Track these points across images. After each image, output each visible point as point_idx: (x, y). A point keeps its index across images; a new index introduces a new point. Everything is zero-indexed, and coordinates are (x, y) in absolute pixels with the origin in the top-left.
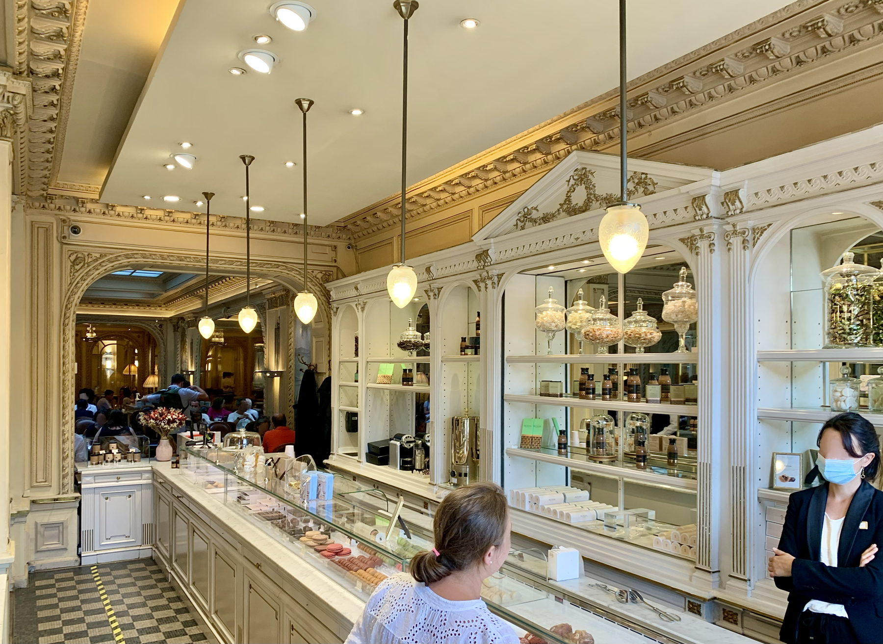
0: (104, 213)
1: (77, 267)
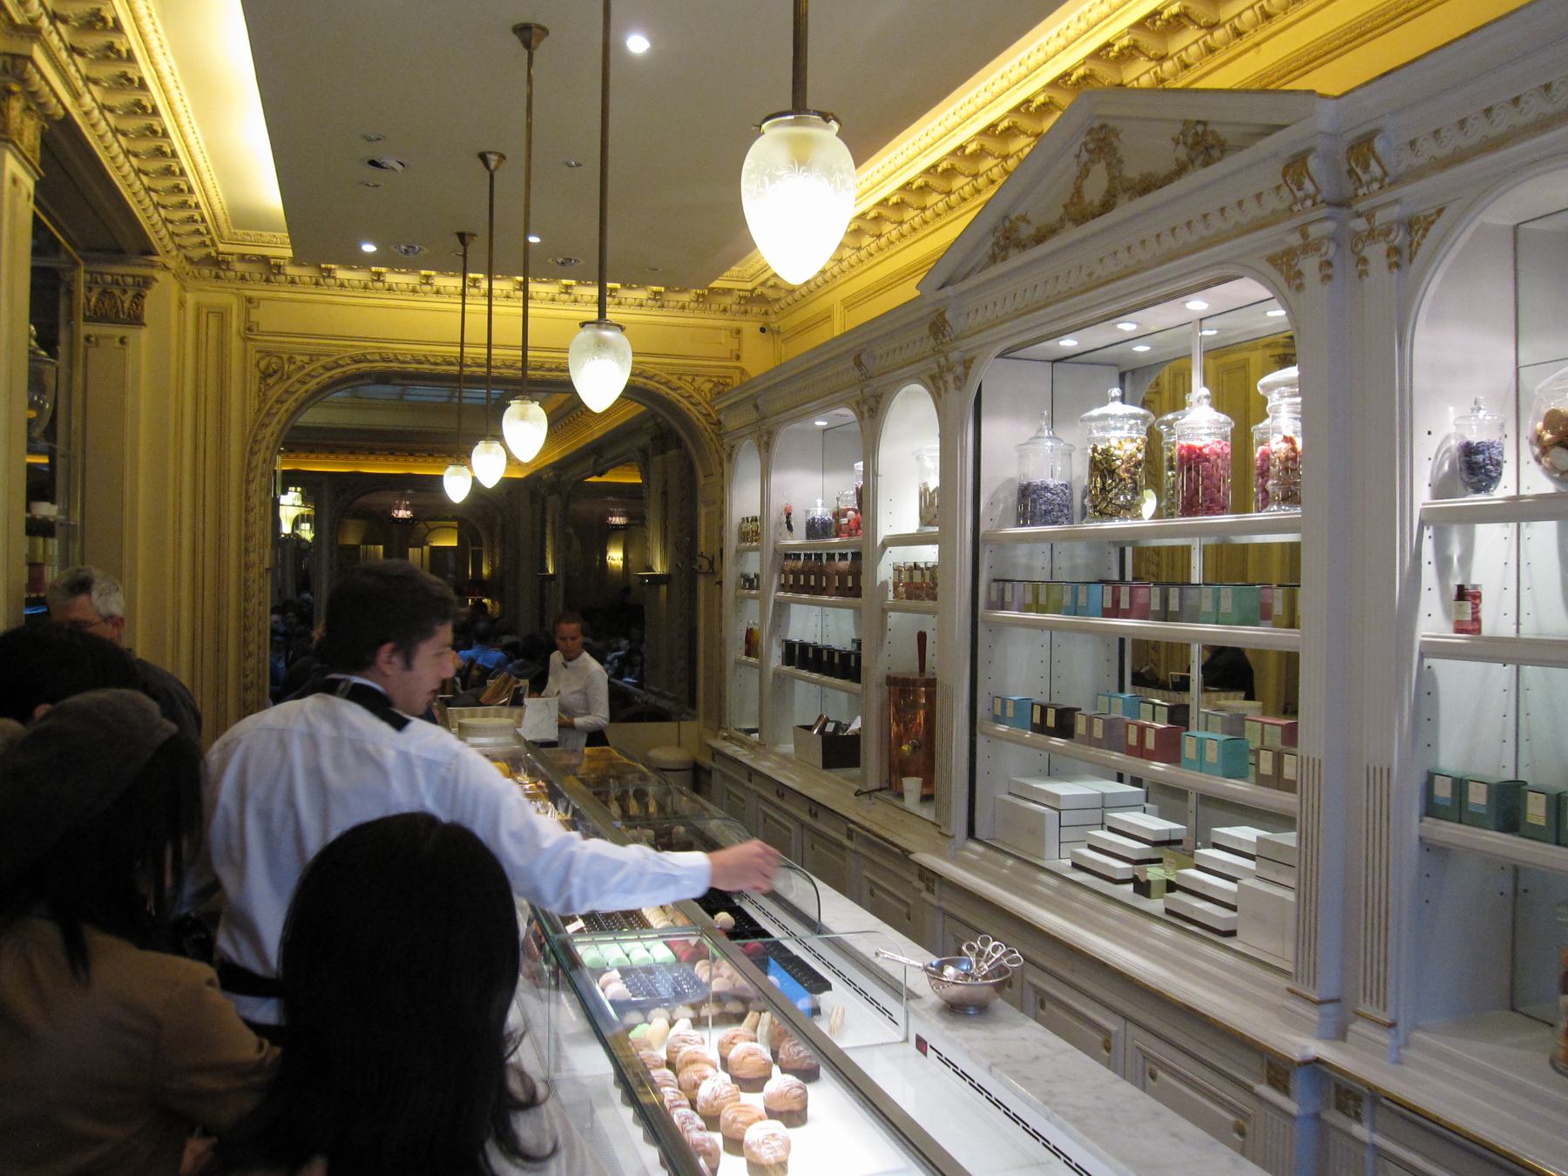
0: (317, 284)
1: (271, 381)
